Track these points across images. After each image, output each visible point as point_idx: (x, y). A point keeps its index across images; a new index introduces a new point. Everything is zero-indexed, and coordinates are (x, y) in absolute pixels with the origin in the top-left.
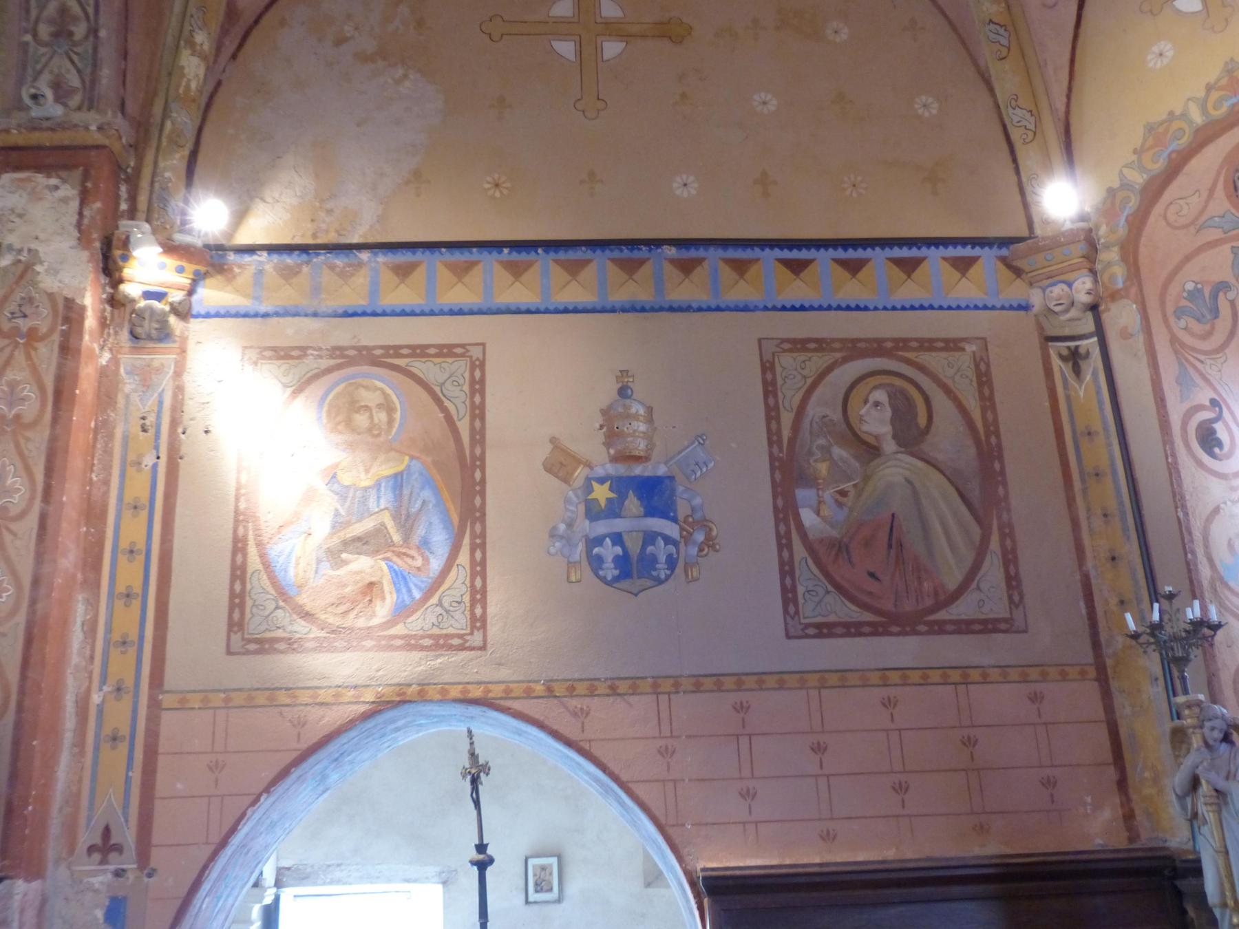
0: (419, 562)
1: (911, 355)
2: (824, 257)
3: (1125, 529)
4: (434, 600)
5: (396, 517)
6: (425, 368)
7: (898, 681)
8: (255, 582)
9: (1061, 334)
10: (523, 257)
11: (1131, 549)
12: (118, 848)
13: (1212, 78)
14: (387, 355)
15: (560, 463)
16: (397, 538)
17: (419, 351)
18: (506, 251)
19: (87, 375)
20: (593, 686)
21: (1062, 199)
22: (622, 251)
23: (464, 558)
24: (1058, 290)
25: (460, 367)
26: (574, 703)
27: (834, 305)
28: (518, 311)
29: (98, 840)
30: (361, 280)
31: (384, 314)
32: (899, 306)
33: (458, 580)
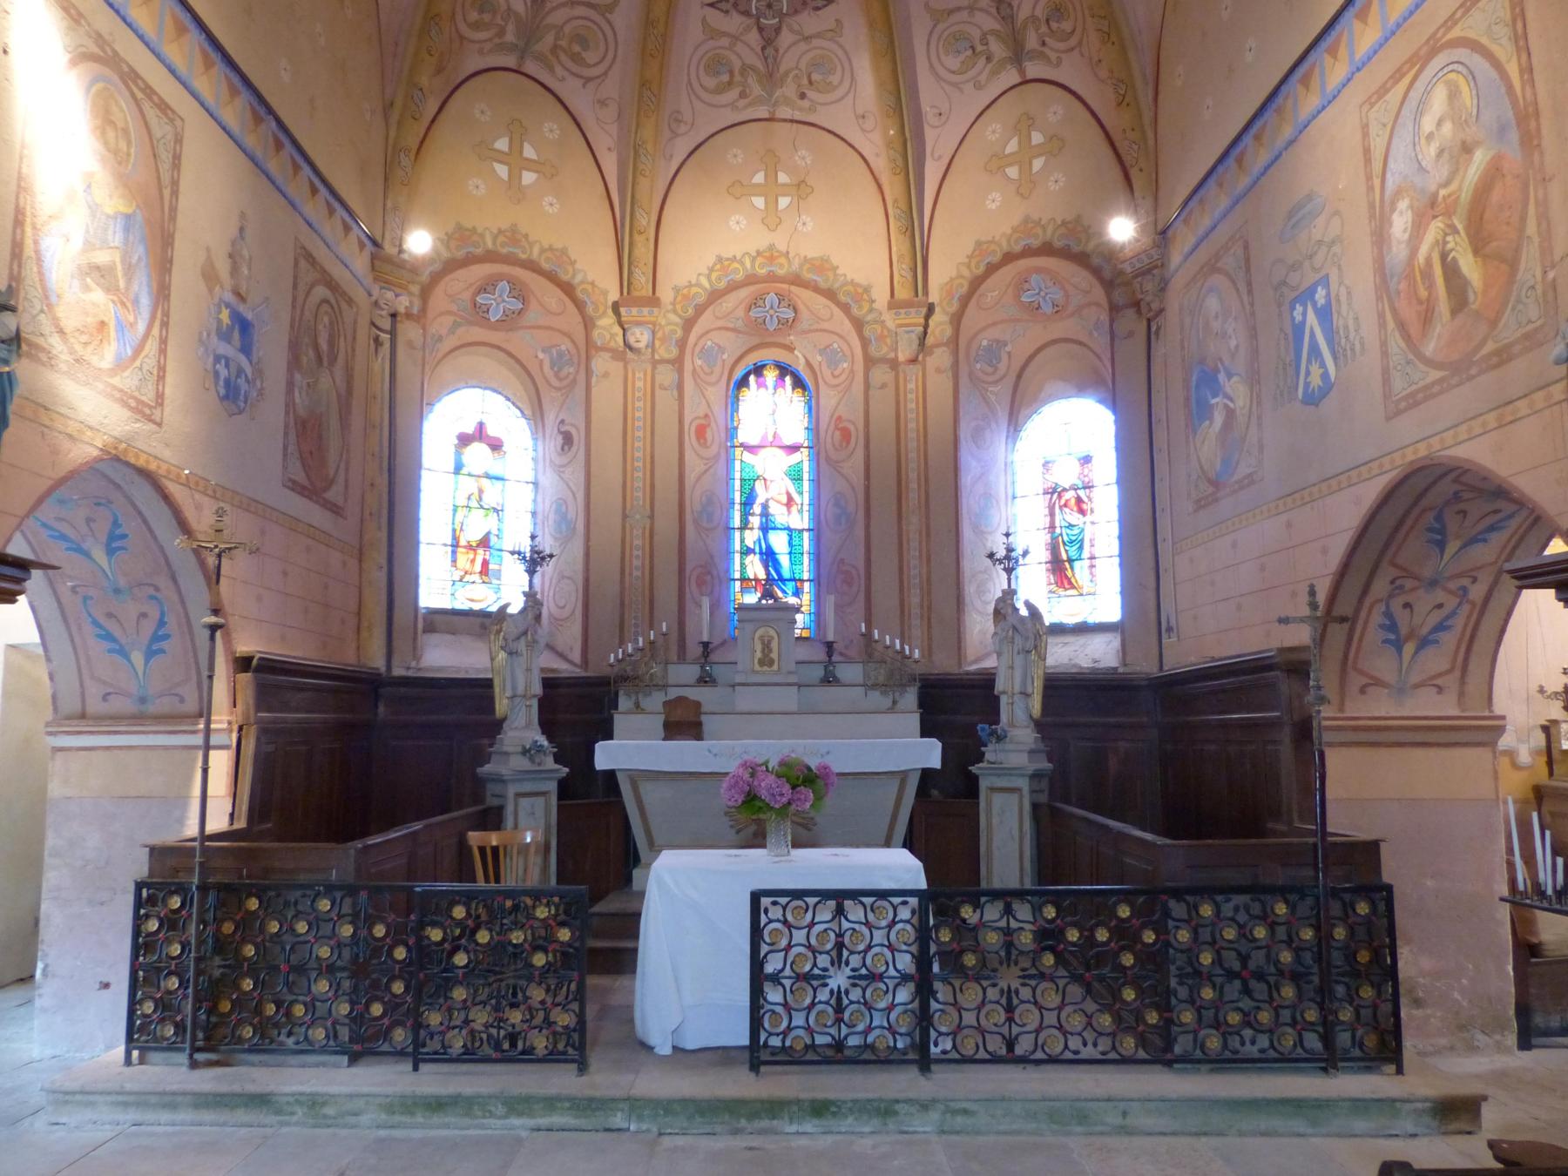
0: (131, 318)
3: (381, 468)
4: (138, 363)
5: (123, 261)
9: (676, 609)
11: (383, 481)
13: (503, 227)
15: (209, 275)
16: (122, 284)
19: (917, 631)
21: (419, 242)
23: (156, 331)
24: (390, 295)
26: (197, 496)
28: (224, 129)
30: (1052, 187)
33: (152, 347)
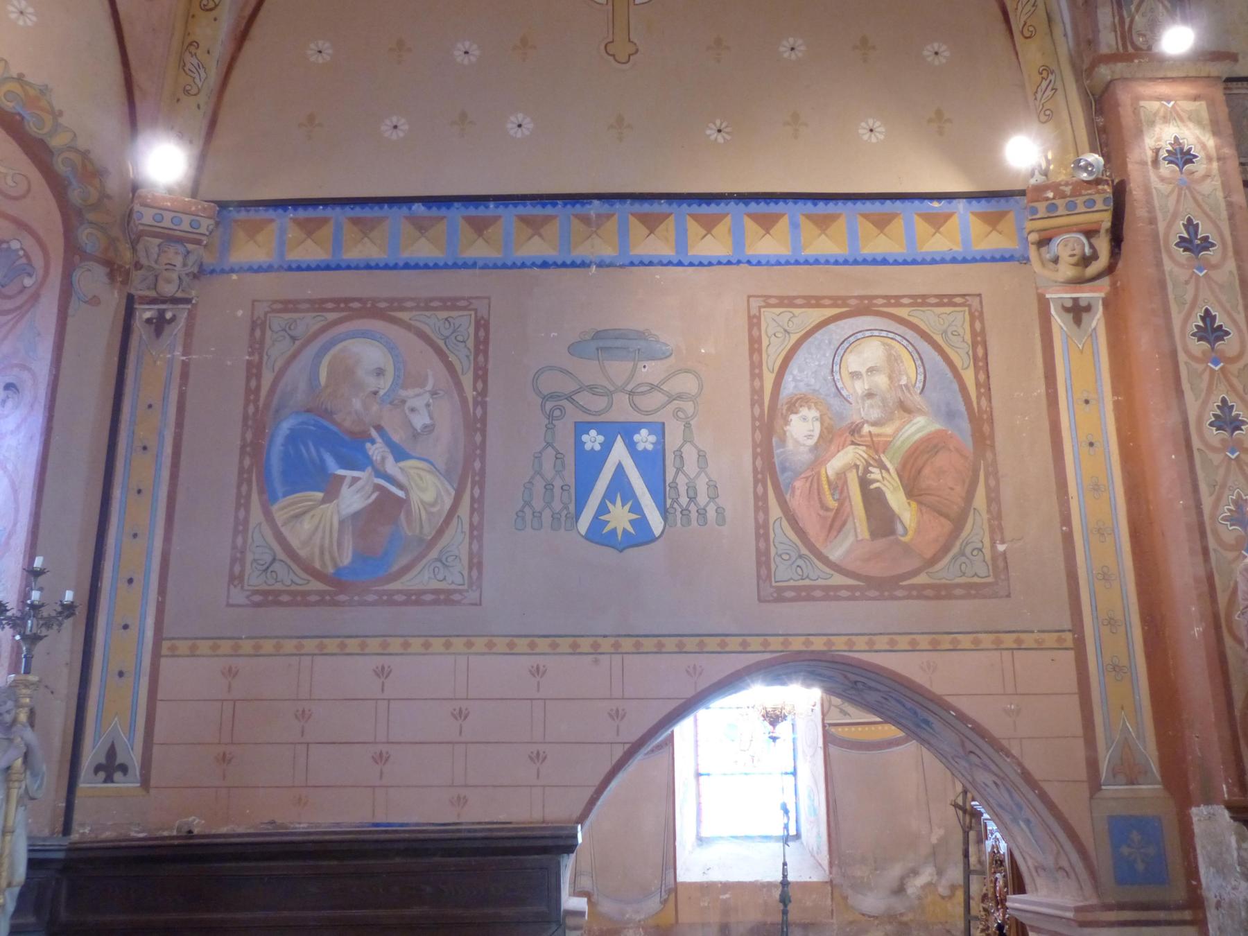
1: (903, 312)
2: (509, 214)
6: (927, 318)
7: (968, 645)
8: (778, 531)
10: (434, 212)
12: (124, 769)
14: (889, 305)
17: (920, 301)
18: (492, 205)
20: (744, 641)
22: (487, 207)
25: (465, 322)
27: (509, 263)
29: (103, 760)
31: (924, 262)
32: (832, 261)
